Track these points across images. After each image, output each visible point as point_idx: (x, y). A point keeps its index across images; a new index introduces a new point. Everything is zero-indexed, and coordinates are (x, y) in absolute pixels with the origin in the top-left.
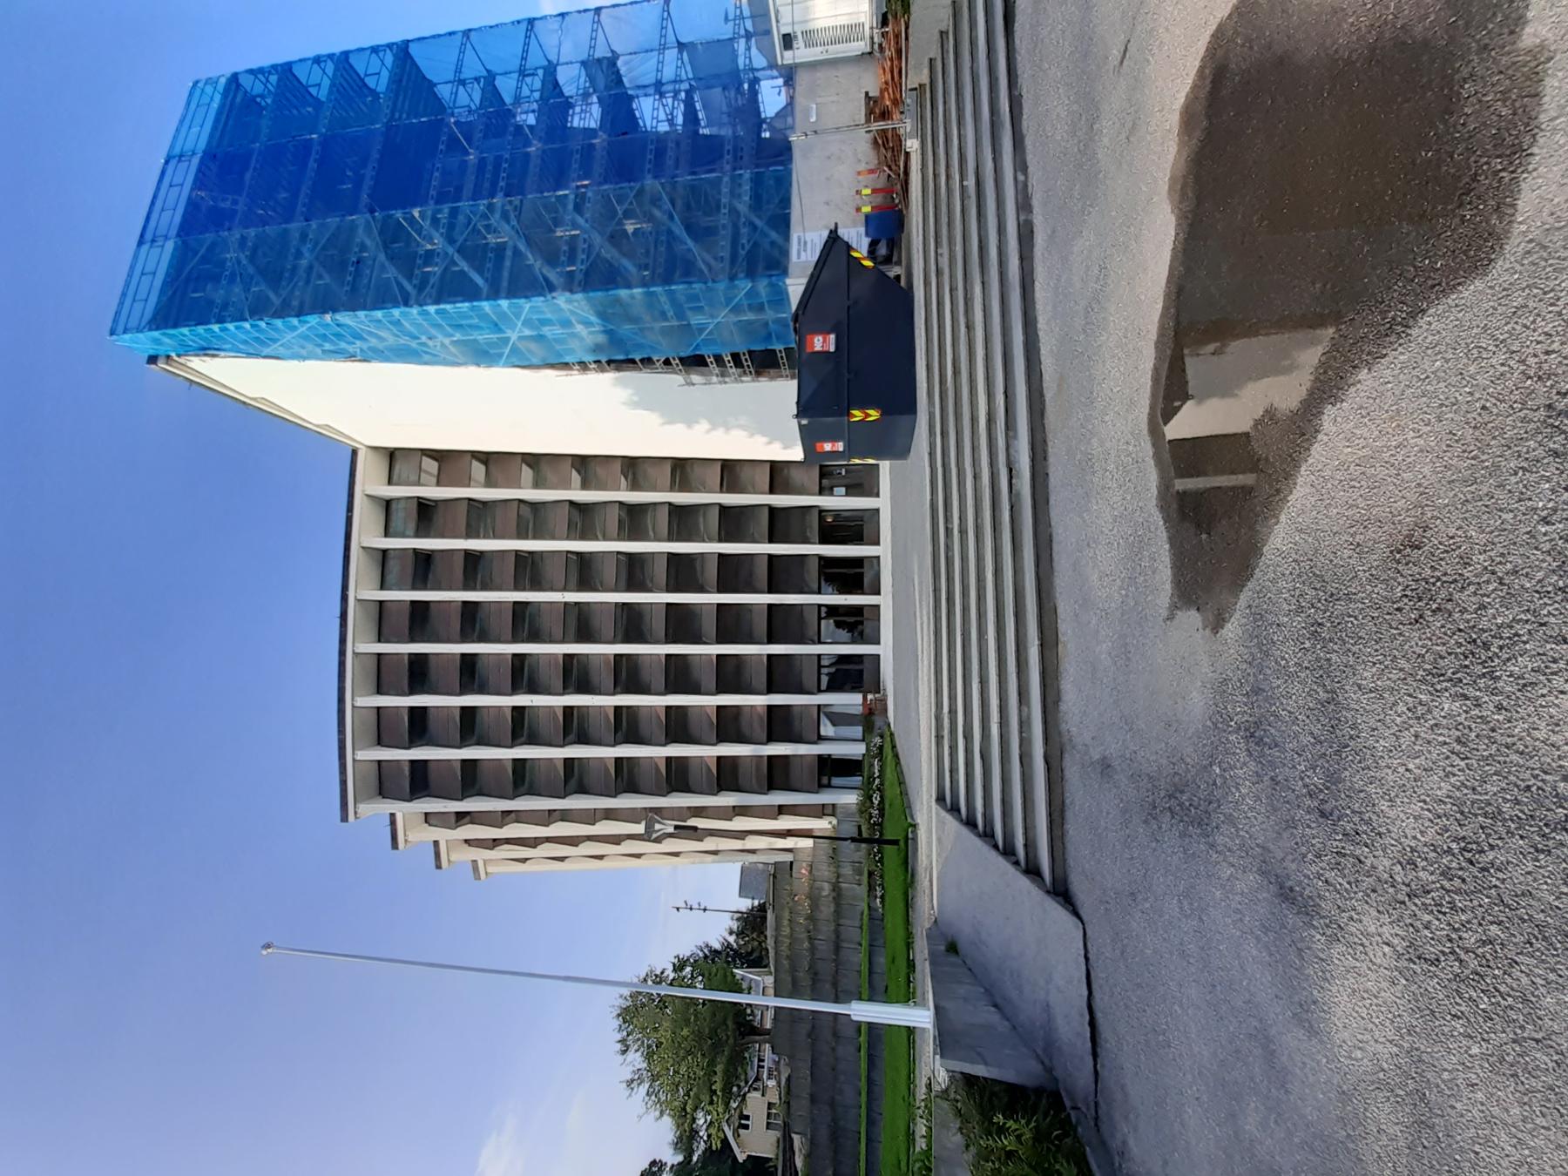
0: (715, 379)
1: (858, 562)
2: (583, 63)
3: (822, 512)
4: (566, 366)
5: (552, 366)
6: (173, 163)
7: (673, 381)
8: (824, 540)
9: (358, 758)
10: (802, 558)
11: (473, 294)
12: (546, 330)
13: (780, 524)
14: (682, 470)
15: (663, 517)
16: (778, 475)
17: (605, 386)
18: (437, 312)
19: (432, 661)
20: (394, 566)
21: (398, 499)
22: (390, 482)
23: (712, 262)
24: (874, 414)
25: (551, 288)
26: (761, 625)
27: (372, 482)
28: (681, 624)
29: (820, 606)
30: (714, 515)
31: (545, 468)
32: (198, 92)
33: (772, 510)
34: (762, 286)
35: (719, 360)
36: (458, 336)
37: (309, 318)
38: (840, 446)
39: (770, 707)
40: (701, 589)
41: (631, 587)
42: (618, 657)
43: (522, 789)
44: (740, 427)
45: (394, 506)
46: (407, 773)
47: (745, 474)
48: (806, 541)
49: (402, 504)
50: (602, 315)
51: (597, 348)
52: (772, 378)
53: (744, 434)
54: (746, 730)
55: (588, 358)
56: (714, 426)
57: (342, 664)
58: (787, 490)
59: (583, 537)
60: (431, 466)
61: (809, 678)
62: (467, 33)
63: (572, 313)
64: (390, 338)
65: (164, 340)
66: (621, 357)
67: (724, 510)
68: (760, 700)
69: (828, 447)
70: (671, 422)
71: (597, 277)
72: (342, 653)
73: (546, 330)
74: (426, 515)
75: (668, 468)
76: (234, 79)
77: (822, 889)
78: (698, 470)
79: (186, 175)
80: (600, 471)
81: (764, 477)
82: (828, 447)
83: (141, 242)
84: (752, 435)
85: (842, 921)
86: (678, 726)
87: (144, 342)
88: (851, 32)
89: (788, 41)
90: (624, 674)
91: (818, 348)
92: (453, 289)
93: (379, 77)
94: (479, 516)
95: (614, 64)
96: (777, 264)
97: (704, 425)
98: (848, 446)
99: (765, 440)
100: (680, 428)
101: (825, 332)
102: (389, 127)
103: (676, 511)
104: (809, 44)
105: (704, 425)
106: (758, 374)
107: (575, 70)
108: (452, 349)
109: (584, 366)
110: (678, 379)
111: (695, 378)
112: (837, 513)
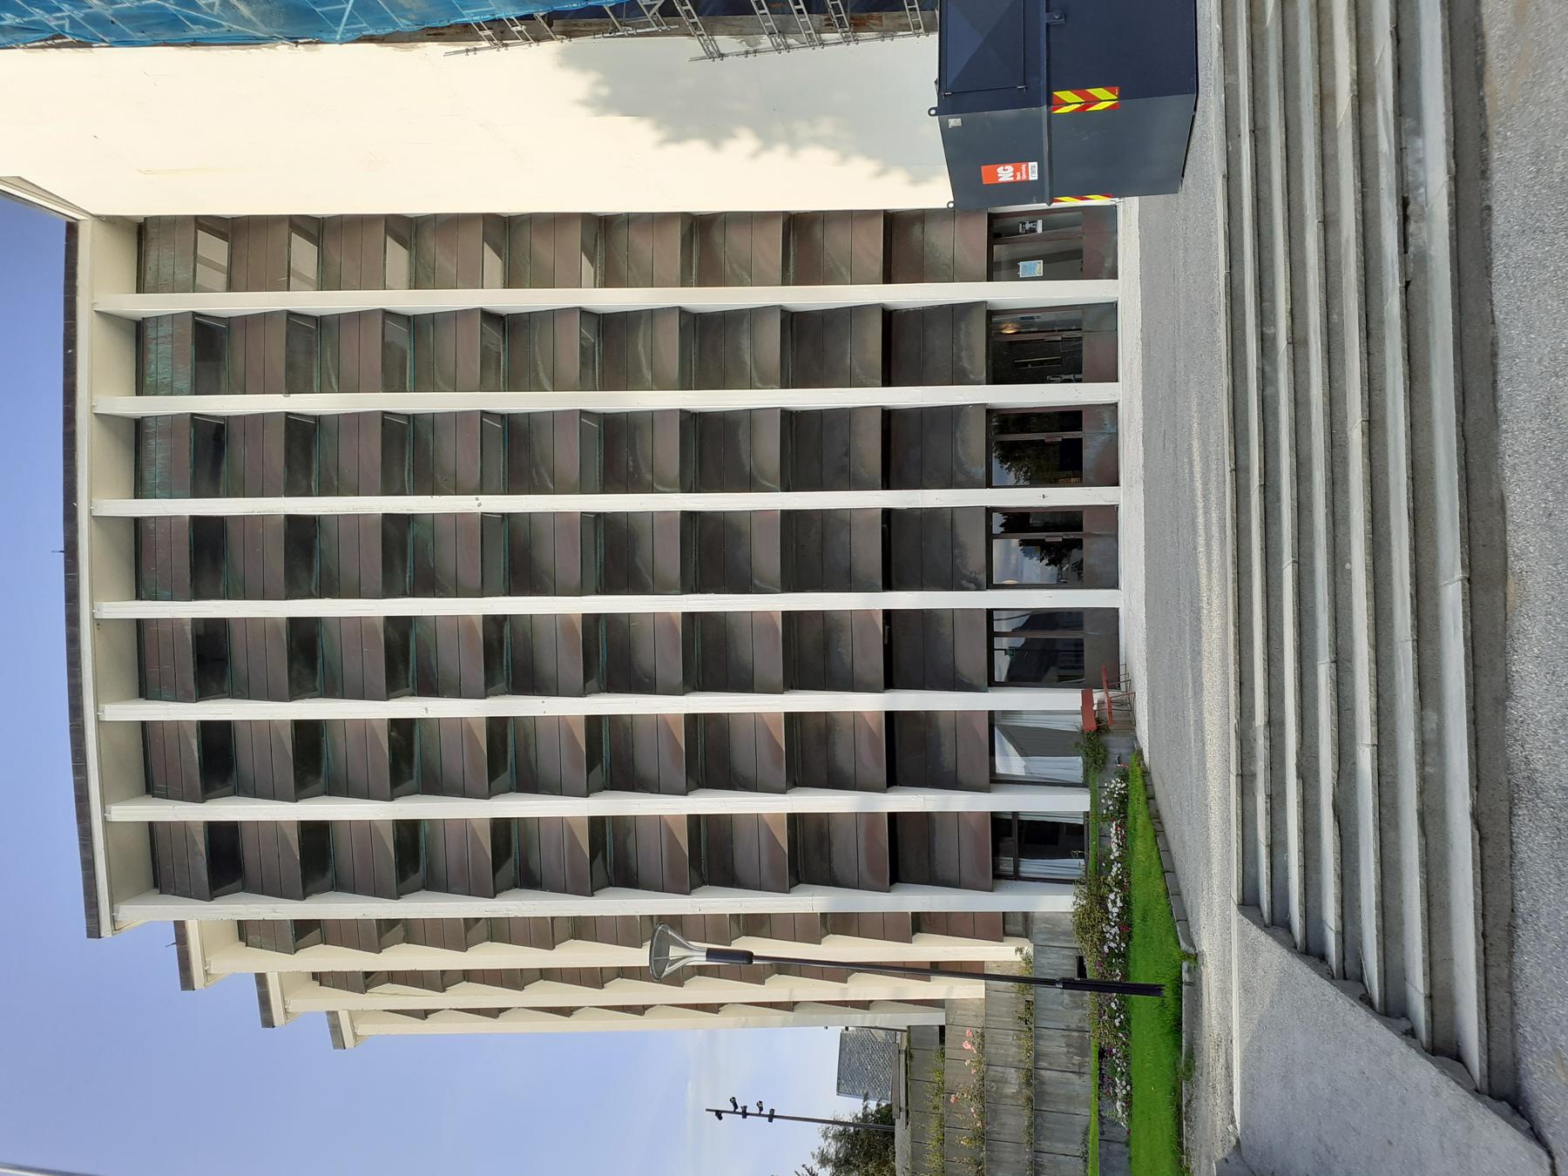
0: (765, 42)
3: (992, 315)
8: (997, 376)
13: (903, 345)
14: (703, 240)
15: (669, 343)
16: (900, 241)
20: (158, 451)
21: (158, 319)
24: (1105, 98)
27: (107, 288)
31: (432, 245)
33: (890, 317)
41: (610, 484)
44: (817, 141)
45: (151, 333)
46: (202, 847)
47: (834, 242)
48: (958, 377)
49: (165, 330)
52: (887, 33)
54: (843, 758)
56: (767, 141)
57: (73, 641)
58: (920, 273)
61: (970, 656)
68: (871, 703)
70: (678, 137)
72: (73, 619)
74: (212, 349)
77: (1003, 1081)
80: (643, 244)
81: (871, 244)
84: (845, 158)
85: (1045, 1145)
94: (310, 348)
100: (696, 150)
106: (858, 25)
110: (690, 46)
111: (725, 42)
112: (1025, 317)
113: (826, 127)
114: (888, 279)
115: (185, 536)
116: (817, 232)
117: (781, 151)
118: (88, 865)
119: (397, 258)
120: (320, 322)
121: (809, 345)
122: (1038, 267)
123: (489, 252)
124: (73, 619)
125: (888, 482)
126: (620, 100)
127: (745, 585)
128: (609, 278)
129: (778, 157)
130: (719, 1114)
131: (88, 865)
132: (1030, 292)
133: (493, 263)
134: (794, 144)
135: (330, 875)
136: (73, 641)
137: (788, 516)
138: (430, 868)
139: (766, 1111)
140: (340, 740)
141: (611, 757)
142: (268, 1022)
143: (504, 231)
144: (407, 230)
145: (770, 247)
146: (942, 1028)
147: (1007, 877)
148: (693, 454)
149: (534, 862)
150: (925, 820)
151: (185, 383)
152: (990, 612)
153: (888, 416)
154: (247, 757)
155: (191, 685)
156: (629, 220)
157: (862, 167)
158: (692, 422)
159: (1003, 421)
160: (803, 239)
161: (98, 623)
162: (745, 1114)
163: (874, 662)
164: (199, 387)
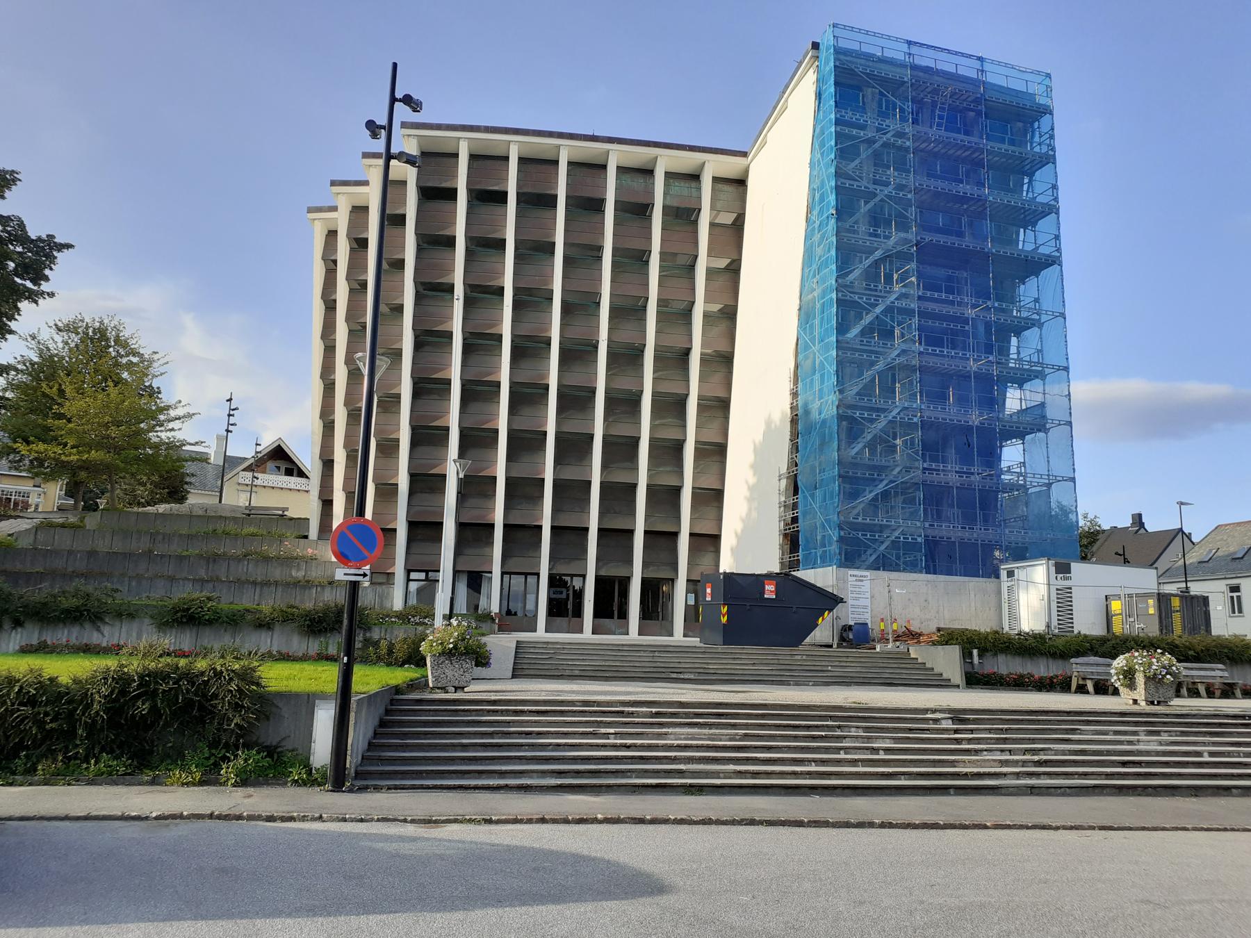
0: (783, 499)
1: (623, 615)
2: (1043, 405)
3: (672, 581)
4: (796, 382)
5: (797, 367)
6: (977, 64)
7: (782, 464)
8: (644, 581)
9: (461, 142)
10: (630, 561)
11: (842, 328)
12: (817, 376)
13: (661, 540)
14: (714, 453)
15: (671, 434)
16: (708, 542)
17: (780, 407)
18: (831, 299)
19: (547, 213)
20: (638, 183)
21: (699, 189)
22: (716, 180)
23: (855, 512)
24: (724, 620)
25: (841, 392)
26: (568, 521)
27: (714, 166)
28: (573, 447)
29: (584, 576)
30: (681, 344)
31: (723, 326)
32: (1039, 79)
33: (675, 535)
34: (834, 548)
35: (795, 506)
36: (818, 306)
37: (834, 196)
38: (708, 598)
39: (492, 526)
40: (605, 466)
41: (609, 401)
42: (547, 387)
43: (421, 289)
44: (750, 510)
45: (694, 184)
46: (444, 185)
47: (711, 512)
48: (645, 564)
49: (694, 193)
50: (824, 421)
51: (807, 412)
52: (782, 547)
53: (744, 515)
54: (471, 502)
55: (800, 401)
56: (751, 489)
57: (550, 134)
58: (693, 549)
59: (657, 358)
60: (728, 219)
61: (516, 564)
62: (1063, 315)
63: (825, 405)
64: (819, 251)
65: (827, 55)
66: (800, 425)
67: (677, 491)
68: (498, 517)
69: (709, 591)
70: (755, 450)
71: (850, 423)
72: (561, 135)
73: (817, 376)
74: (683, 217)
75: (719, 440)
76: (1047, 111)
77: (298, 570)
78: (715, 468)
79: (968, 70)
80: (718, 377)
81: (706, 528)
82: (709, 591)
83: (909, 43)
84: (743, 521)
85: (280, 589)
86: (477, 440)
87: (827, 40)
88: (1014, 617)
89: (1011, 574)
90: (528, 390)
91: (767, 587)
92: (847, 309)
93: (1026, 241)
94: (680, 268)
95: (1039, 430)
96: (851, 556)
97: (752, 480)
98: (709, 604)
99: (739, 531)
100: (751, 458)
101: (777, 592)
102: (986, 256)
103: (679, 446)
104: (1010, 589)
105: (752, 480)
106: (785, 535)
107: (1039, 398)
108: (810, 297)
109: (795, 395)
110: (784, 470)
111: (784, 482)
112: (670, 596)
113: (754, 514)
114: (691, 535)
115: (597, 195)
116: (716, 504)
117: (747, 494)
118: (439, 127)
119: (722, 263)
120: (695, 223)
121: (665, 497)
122: (691, 602)
123: (729, 261)
124: (561, 135)
125: (601, 531)
126: (769, 430)
127: (558, 461)
128: (704, 360)
129: (745, 492)
130: (230, 400)
131: (439, 127)
132: (680, 597)
133: (716, 307)
134: (750, 500)
135: (425, 246)
136: (550, 134)
137: (588, 484)
138: (426, 296)
139: (231, 428)
140: (494, 259)
141: (478, 392)
142: (333, 183)
143: (729, 315)
144: (734, 270)
145: (709, 482)
146: (306, 537)
147: (408, 575)
148: (620, 440)
149: (427, 348)
150: (438, 539)
151: (668, 203)
152: (538, 575)
153: (631, 532)
154: (487, 210)
155: (525, 190)
156: (727, 418)
157: (739, 527)
158: (635, 441)
159: (625, 582)
160: (711, 498)
161: (558, 147)
162: (229, 415)
163: (517, 520)
164: (666, 210)
